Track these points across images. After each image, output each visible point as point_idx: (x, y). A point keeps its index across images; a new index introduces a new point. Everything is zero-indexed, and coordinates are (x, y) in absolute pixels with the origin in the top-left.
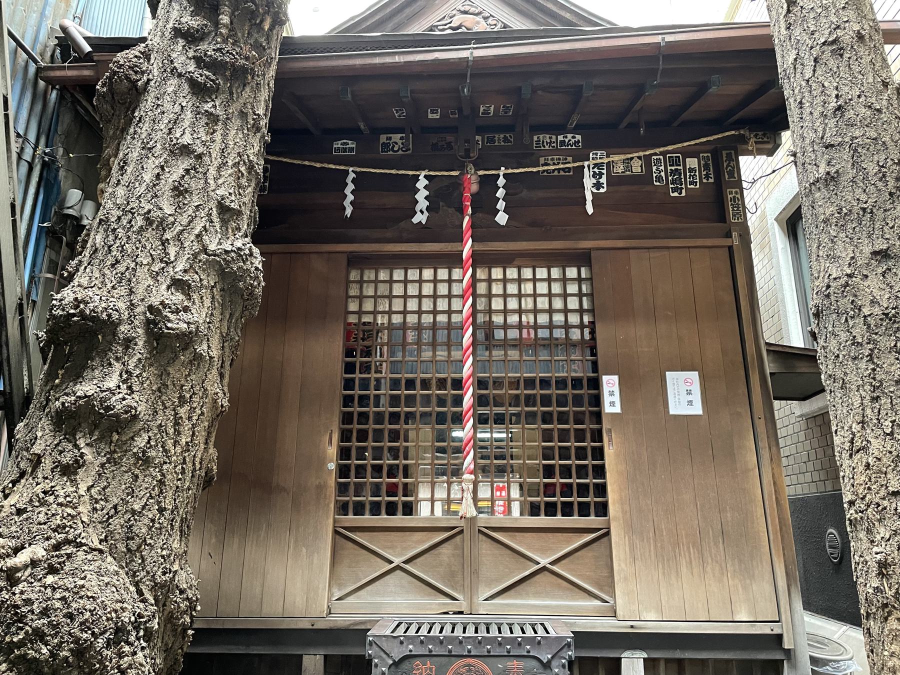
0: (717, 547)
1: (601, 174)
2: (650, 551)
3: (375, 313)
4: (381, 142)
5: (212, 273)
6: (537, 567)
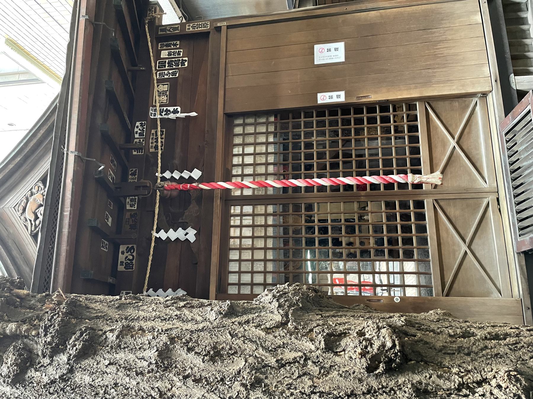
0: (434, 32)
1: (167, 111)
2: (442, 71)
4: (124, 270)
5: (306, 317)
6: (457, 148)
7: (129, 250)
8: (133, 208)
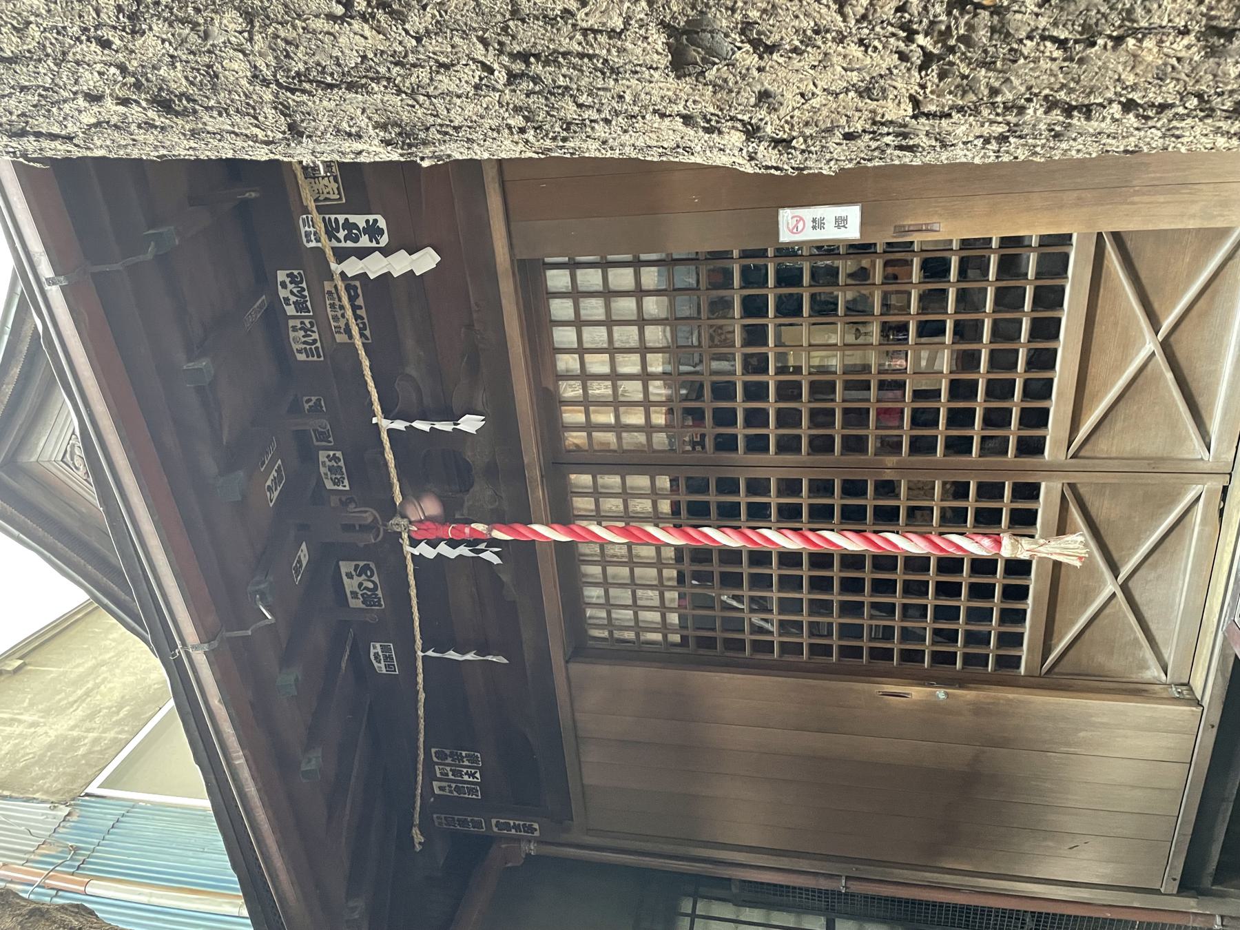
1: (348, 225)
7: (361, 571)
8: (341, 488)
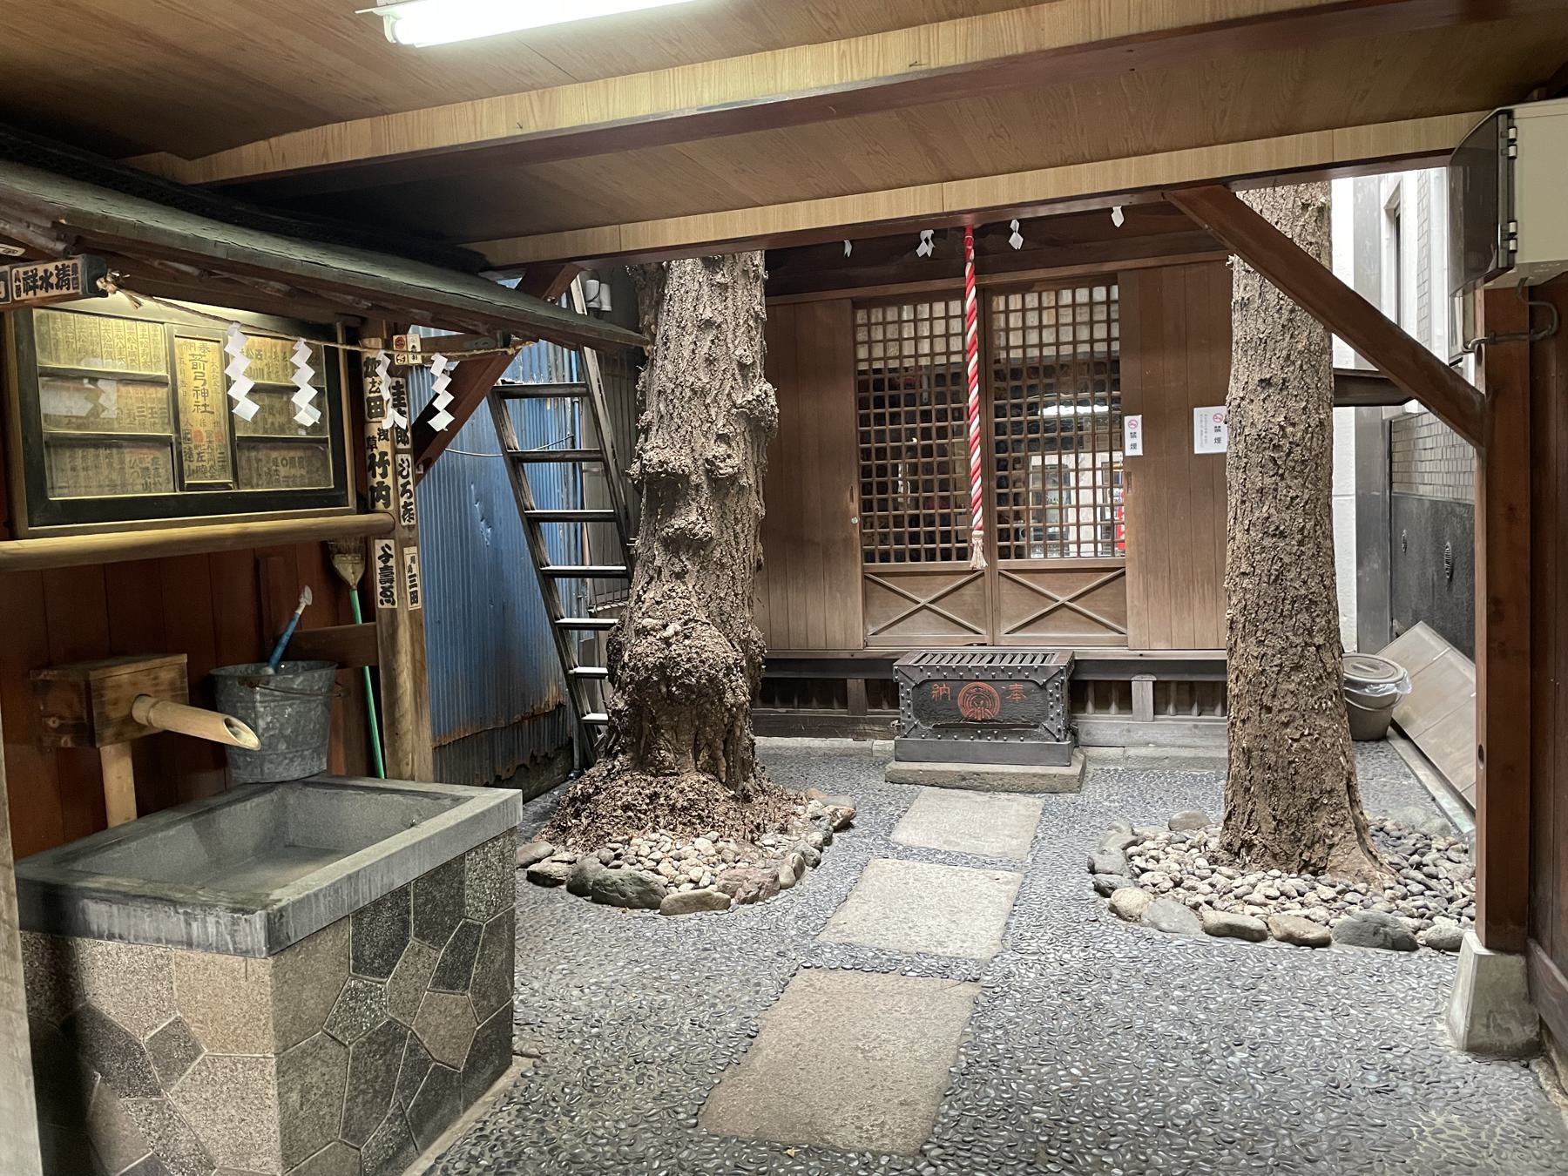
3: (885, 359)
